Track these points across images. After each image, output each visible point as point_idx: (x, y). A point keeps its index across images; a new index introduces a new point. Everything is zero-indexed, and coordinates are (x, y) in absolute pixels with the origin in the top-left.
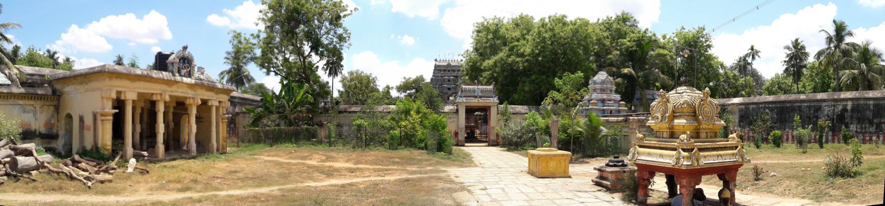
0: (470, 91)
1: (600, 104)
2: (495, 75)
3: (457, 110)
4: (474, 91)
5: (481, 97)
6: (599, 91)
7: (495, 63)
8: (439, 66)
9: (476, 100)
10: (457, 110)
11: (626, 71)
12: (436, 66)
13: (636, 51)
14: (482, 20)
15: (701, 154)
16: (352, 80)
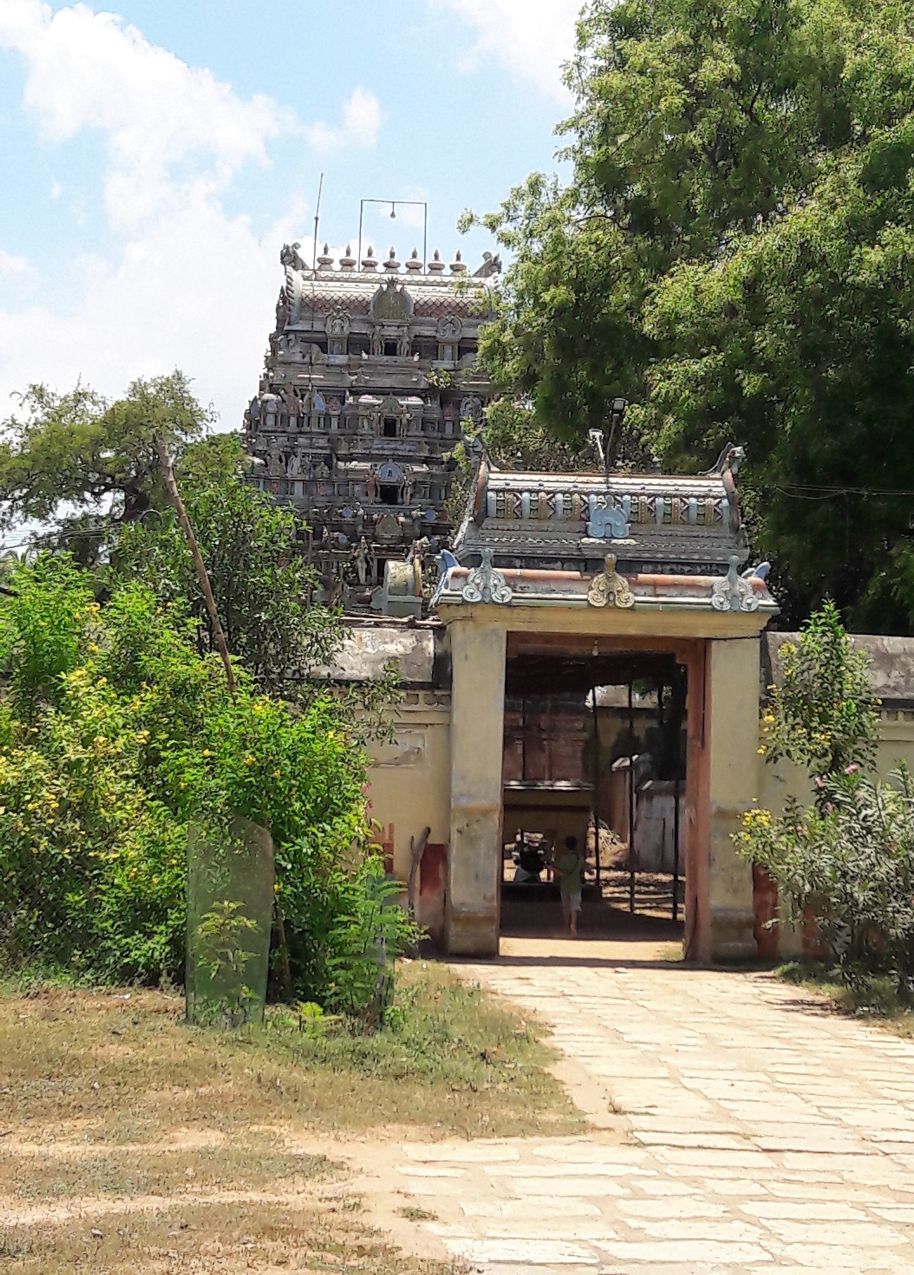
0: (543, 510)
2: (751, 383)
4: (580, 516)
5: (628, 566)
7: (751, 286)
8: (313, 305)
9: (592, 592)
12: (288, 307)
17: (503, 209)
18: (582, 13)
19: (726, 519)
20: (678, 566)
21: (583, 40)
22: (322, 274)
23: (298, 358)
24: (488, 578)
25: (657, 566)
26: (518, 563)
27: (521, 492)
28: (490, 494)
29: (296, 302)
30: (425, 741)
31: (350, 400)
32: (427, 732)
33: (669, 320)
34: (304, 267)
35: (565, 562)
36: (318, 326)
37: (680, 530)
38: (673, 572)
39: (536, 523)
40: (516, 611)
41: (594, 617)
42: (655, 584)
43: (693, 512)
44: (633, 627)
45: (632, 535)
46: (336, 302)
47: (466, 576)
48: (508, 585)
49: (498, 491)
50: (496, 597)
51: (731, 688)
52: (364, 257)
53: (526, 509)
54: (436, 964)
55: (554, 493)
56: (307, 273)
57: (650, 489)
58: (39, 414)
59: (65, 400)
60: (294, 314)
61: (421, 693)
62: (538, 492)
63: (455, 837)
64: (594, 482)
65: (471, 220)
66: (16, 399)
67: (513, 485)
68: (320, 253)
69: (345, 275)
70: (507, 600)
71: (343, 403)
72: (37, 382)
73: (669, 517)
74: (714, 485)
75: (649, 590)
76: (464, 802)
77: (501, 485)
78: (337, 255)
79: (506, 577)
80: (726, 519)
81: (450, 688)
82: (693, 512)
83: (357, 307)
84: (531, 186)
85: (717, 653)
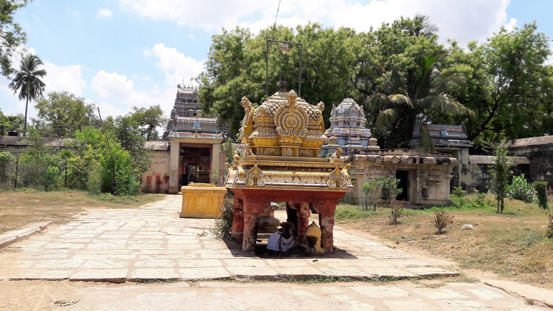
0: (186, 123)
1: (342, 141)
2: (229, 105)
3: (169, 148)
4: (192, 124)
5: (200, 132)
6: (341, 124)
7: (230, 90)
8: (182, 94)
10: (169, 148)
11: (394, 98)
13: (415, 69)
14: (221, 33)
15: (264, 172)
16: (54, 105)
21: (211, 50)
25: (205, 132)
30: (166, 160)
33: (217, 94)
35: (190, 131)
44: (200, 142)
51: (216, 152)
54: (539, 290)
74: (215, 120)
78: (187, 86)
83: (190, 95)
85: (214, 146)
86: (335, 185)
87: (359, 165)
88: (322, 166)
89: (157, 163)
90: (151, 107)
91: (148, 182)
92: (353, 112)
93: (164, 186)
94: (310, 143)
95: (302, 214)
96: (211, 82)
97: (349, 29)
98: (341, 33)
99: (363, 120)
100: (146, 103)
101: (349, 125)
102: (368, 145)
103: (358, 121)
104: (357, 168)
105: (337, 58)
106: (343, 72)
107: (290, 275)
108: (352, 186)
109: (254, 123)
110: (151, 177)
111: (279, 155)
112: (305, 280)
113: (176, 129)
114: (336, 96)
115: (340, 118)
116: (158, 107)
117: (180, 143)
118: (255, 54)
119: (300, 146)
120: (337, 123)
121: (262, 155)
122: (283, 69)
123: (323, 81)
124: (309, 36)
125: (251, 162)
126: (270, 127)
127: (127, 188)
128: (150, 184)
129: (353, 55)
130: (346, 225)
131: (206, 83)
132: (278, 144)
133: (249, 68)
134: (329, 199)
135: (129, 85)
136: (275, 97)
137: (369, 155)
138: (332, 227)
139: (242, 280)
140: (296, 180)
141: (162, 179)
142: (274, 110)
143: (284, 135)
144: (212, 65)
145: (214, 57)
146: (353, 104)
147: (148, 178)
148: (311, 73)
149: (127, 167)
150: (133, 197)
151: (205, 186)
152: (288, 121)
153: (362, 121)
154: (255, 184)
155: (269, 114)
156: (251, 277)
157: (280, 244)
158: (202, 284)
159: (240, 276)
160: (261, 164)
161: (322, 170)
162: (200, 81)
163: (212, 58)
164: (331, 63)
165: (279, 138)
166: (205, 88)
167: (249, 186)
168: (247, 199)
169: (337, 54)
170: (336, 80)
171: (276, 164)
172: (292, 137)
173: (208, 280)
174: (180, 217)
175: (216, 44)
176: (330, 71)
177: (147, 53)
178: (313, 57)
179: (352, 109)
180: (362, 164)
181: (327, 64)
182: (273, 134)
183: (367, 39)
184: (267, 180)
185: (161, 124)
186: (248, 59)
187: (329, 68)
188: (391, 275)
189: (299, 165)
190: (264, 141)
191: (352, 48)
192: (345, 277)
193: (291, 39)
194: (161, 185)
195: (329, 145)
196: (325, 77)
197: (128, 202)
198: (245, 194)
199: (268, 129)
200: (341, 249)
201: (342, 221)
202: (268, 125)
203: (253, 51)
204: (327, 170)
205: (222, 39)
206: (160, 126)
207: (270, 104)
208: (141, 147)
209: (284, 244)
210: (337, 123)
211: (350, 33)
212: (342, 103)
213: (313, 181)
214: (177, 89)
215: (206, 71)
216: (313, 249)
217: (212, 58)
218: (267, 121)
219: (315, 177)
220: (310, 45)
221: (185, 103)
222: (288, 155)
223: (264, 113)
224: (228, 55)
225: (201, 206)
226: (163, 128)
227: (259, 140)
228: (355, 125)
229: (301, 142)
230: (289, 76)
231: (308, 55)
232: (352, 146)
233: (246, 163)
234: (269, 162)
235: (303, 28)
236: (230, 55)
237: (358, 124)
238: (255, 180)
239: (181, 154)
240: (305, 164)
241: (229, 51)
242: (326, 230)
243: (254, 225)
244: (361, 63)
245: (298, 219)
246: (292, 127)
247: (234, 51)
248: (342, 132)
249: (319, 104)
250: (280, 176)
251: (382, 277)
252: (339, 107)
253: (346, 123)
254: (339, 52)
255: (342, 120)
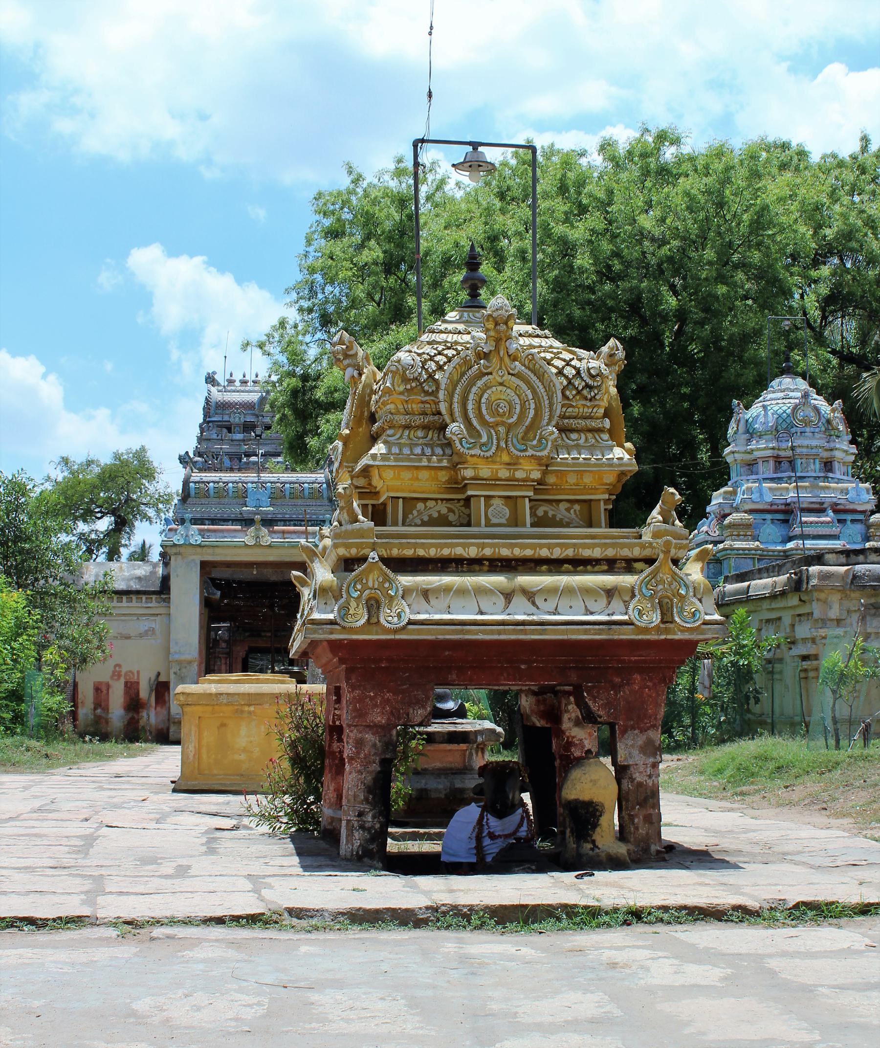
0: (221, 493)
1: (771, 530)
3: (165, 581)
4: (242, 495)
5: (269, 522)
6: (767, 469)
8: (223, 406)
9: (247, 537)
10: (165, 581)
12: (211, 409)
14: (344, 182)
15: (406, 580)
17: (266, 337)
18: (311, 227)
19: (325, 495)
20: (298, 522)
21: (309, 242)
22: (229, 388)
23: (215, 436)
24: (188, 530)
25: (286, 522)
26: (207, 522)
27: (209, 483)
28: (191, 484)
29: (213, 404)
30: (156, 624)
31: (245, 460)
32: (158, 618)
34: (219, 384)
35: (235, 521)
36: (226, 418)
37: (300, 502)
38: (295, 525)
39: (218, 500)
40: (205, 549)
41: (249, 551)
42: (283, 532)
43: (306, 492)
45: (271, 505)
46: (236, 404)
47: (176, 530)
48: (200, 534)
49: (195, 483)
50: (192, 541)
52: (254, 378)
53: (212, 492)
55: (227, 483)
56: (220, 388)
57: (283, 479)
58: (66, 474)
59: (81, 464)
60: (212, 411)
61: (154, 597)
62: (218, 483)
63: (172, 676)
64: (252, 476)
65: (248, 344)
66: (53, 466)
67: (205, 479)
68: (228, 377)
69: (242, 388)
70: (198, 543)
71: (240, 461)
72: (65, 455)
73: (293, 495)
75: (280, 535)
76: (177, 657)
77: (198, 479)
78: (238, 377)
79: (200, 530)
80: (325, 495)
81: (169, 594)
82: (306, 492)
84: (280, 324)
86: (656, 618)
87: (825, 602)
88: (610, 553)
89: (128, 638)
90: (117, 456)
91: (97, 705)
92: (807, 422)
93: (151, 717)
94: (572, 479)
95: (569, 744)
96: (313, 352)
97: (785, 146)
98: (754, 157)
99: (844, 449)
100: (93, 439)
101: (793, 470)
102: (867, 539)
103: (825, 455)
104: (817, 614)
105: (747, 244)
106: (772, 291)
107: (471, 908)
108: (717, 617)
109: (373, 418)
110: (108, 686)
111: (462, 525)
112: (526, 922)
113: (188, 516)
114: (750, 374)
115: (761, 447)
116: (140, 455)
117: (204, 565)
118: (457, 244)
119: (536, 491)
120: (751, 466)
121: (404, 525)
122: (558, 286)
123: (701, 323)
124: (646, 173)
125: (359, 546)
126: (426, 427)
127: (18, 718)
128: (106, 709)
129: (802, 229)
130: (757, 798)
131: (296, 358)
132: (457, 485)
133: (439, 292)
134: (643, 669)
135: (51, 391)
136: (443, 327)
137: (858, 567)
138: (655, 766)
139: (304, 923)
140: (519, 601)
141: (144, 692)
142: (440, 368)
143: (476, 451)
144: (313, 293)
145: (319, 264)
146: (806, 395)
147: (97, 689)
148: (657, 299)
149: (15, 645)
150: (33, 743)
151: (258, 681)
152: (489, 403)
153: (838, 454)
154: (372, 622)
155: (420, 384)
156: (337, 915)
157: (479, 839)
158: (158, 932)
159: (297, 913)
160: (395, 552)
161: (611, 565)
162: (275, 349)
163: (312, 270)
164: (723, 259)
165: (456, 462)
166: (292, 374)
167: (352, 630)
168: (348, 679)
169: (744, 229)
170: (745, 317)
171: (446, 552)
172: (505, 458)
173: (187, 922)
174: (175, 791)
175: (327, 222)
176: (722, 289)
177: (107, 280)
178: (663, 242)
179: (800, 414)
180: (835, 598)
181: (710, 263)
182: (438, 451)
183: (850, 176)
184: (415, 607)
185: (151, 512)
186: (434, 261)
187: (721, 279)
188: (830, 899)
189: (528, 553)
190: (406, 475)
191: (794, 206)
192: (665, 909)
193: (581, 184)
194: (144, 714)
195: (727, 543)
196: (706, 310)
197: (16, 757)
198: (342, 661)
199: (420, 433)
200: (685, 845)
201: (744, 788)
202: (418, 420)
203: (453, 235)
204: (629, 566)
205: (345, 203)
206: (149, 519)
207: (428, 349)
208: (69, 579)
209: (492, 836)
210: (751, 466)
211: (791, 159)
212: (766, 395)
213: (578, 604)
214: (205, 387)
215: (293, 315)
216: (589, 846)
217: (312, 270)
218: (416, 407)
219: (587, 591)
220: (649, 205)
221: (227, 429)
222: (494, 521)
223: (405, 380)
224: (366, 256)
225: (245, 750)
226: (159, 526)
227: (389, 474)
228: (815, 468)
229: (536, 475)
230: (577, 313)
231: (642, 235)
232: (809, 543)
233: (342, 551)
234: (423, 546)
235: (622, 147)
236: (374, 253)
237: (828, 465)
238: (373, 606)
239: (207, 603)
240: (550, 547)
241: (372, 242)
242: (632, 780)
243: (375, 767)
244: (836, 261)
245: (557, 763)
246: (503, 423)
247: (390, 239)
248: (769, 497)
249: (605, 349)
250: (462, 592)
251: (797, 906)
252: (756, 409)
253: (784, 465)
254: (752, 222)
255: (769, 453)
